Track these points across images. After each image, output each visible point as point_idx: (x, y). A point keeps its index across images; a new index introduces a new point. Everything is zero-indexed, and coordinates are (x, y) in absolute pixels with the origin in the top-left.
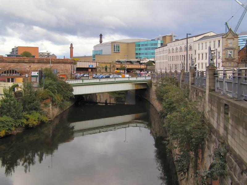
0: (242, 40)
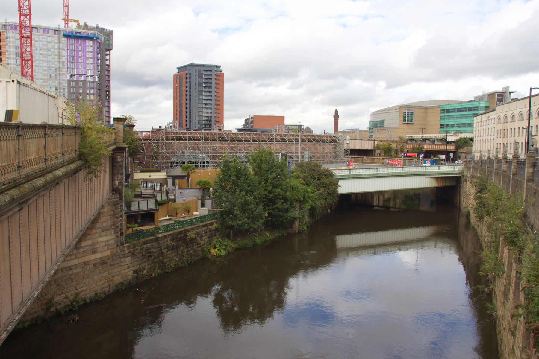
0: (92, 200)
